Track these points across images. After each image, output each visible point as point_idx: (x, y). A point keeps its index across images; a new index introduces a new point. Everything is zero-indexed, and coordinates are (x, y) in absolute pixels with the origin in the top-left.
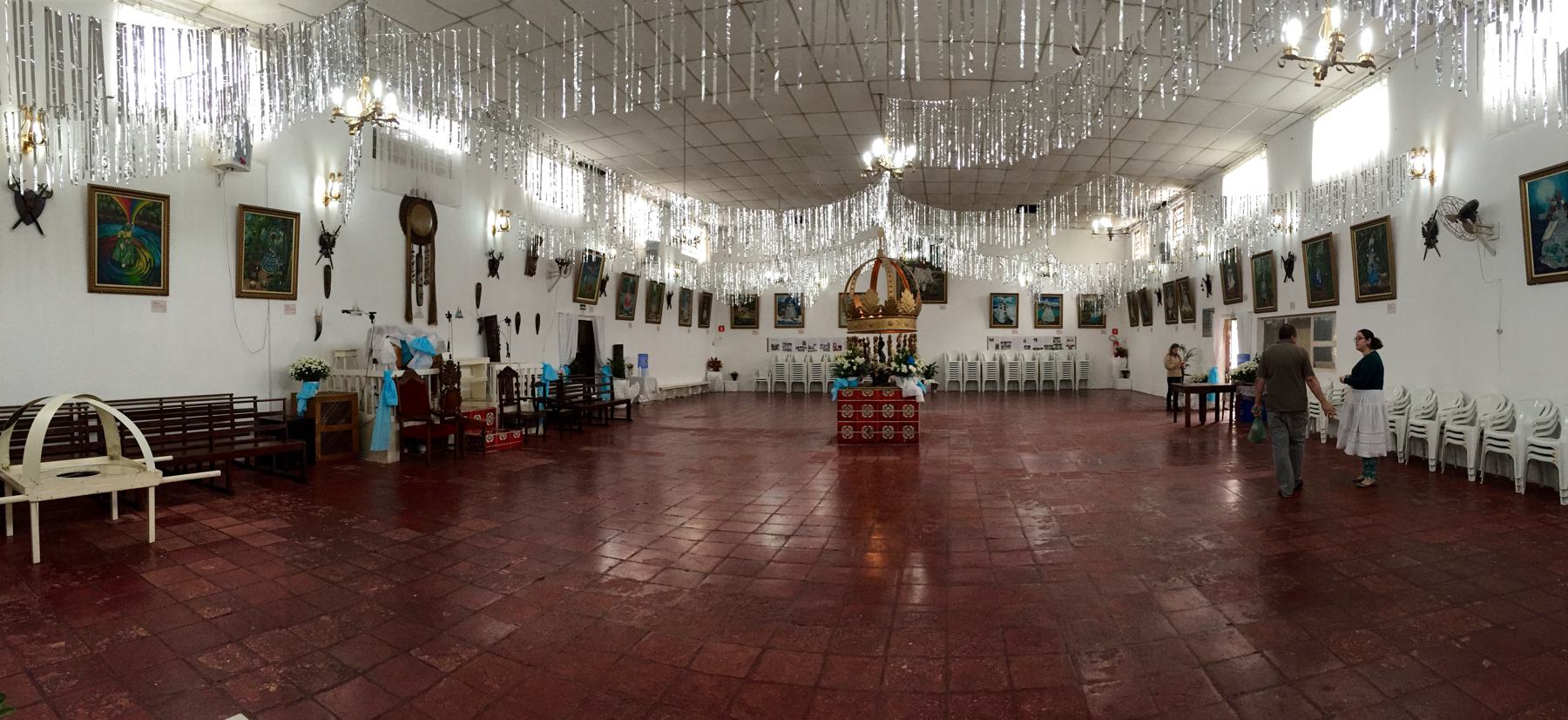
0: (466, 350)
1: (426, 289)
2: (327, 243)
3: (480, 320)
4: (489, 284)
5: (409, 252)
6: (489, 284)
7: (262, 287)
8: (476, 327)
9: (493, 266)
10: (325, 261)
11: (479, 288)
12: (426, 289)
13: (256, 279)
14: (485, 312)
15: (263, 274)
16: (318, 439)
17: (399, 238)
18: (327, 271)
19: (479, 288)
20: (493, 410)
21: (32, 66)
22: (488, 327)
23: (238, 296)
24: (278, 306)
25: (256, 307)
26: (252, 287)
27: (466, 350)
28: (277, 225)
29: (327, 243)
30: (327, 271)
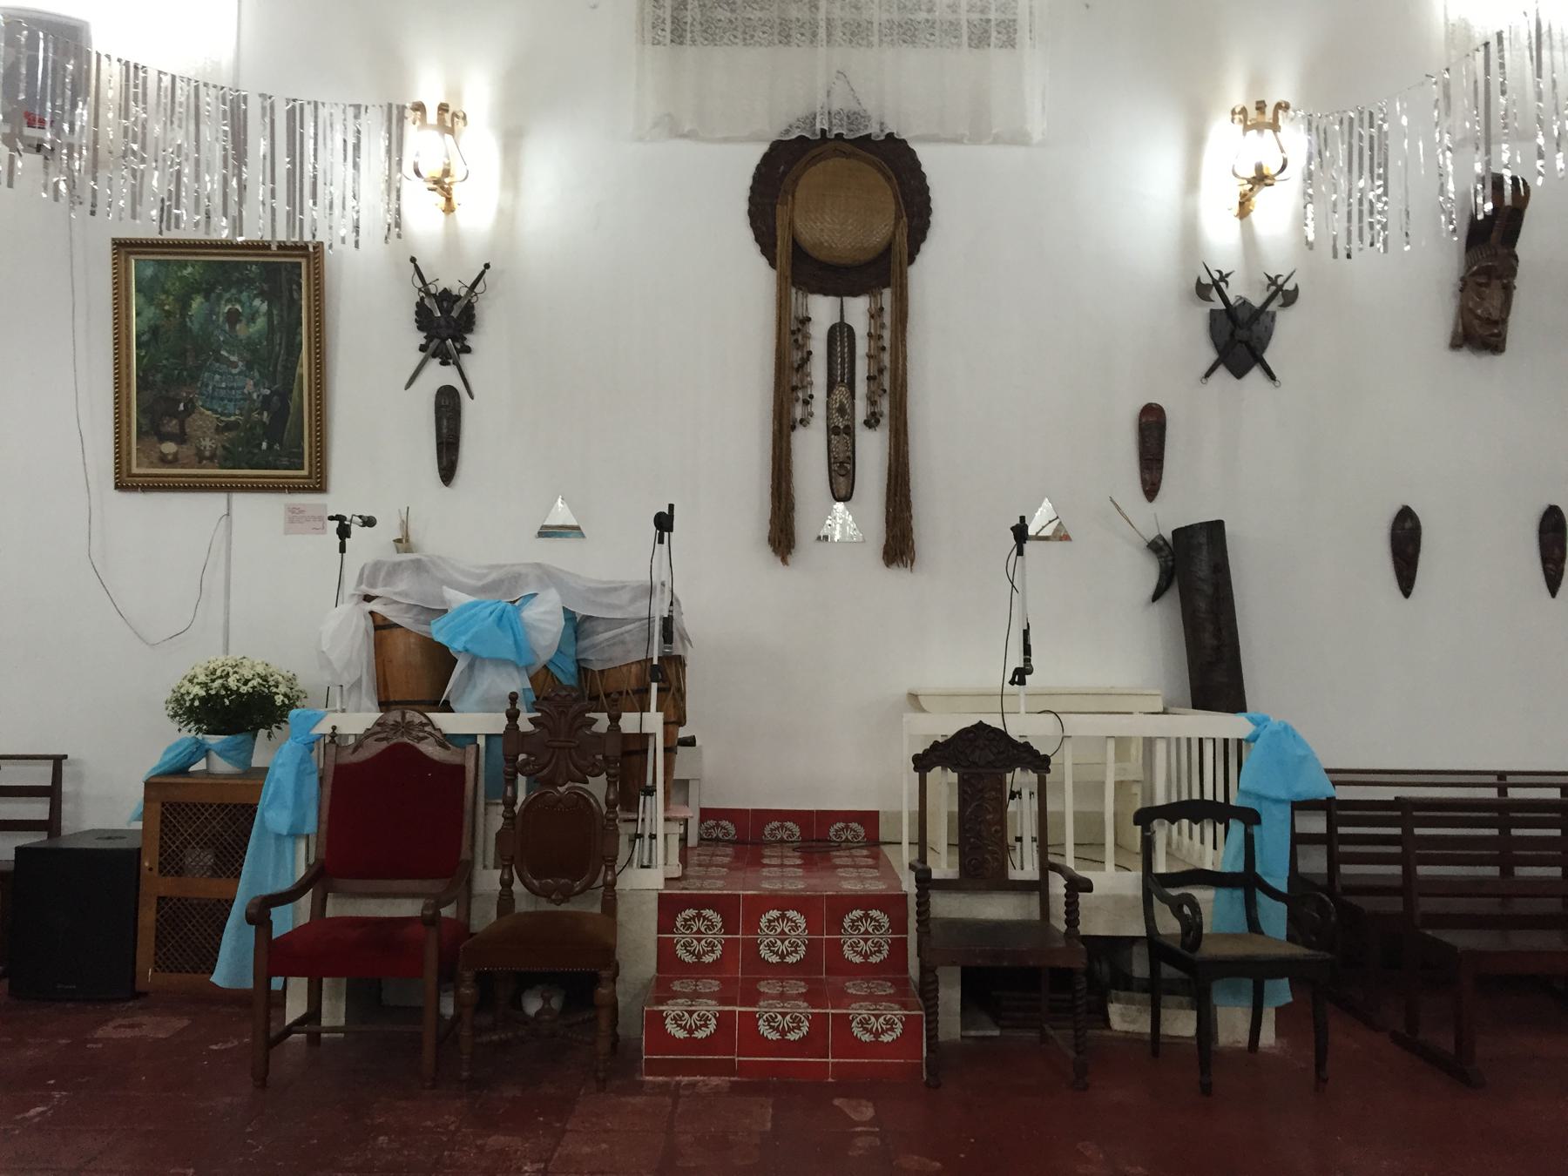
0: (1100, 689)
1: (871, 448)
2: (446, 321)
3: (1155, 546)
4: (1209, 412)
5: (790, 335)
6: (1209, 412)
7: (201, 458)
8: (1147, 572)
9: (1239, 335)
10: (439, 374)
11: (1152, 427)
12: (871, 448)
13: (181, 438)
14: (1178, 508)
15: (203, 423)
16: (148, 918)
17: (752, 279)
18: (448, 407)
19: (1152, 427)
20: (893, 904)
21: (225, 167)
22: (1194, 571)
23: (121, 486)
24: (259, 515)
25: (187, 518)
26: (164, 460)
27: (1100, 689)
28: (244, 283)
29: (446, 321)
30: (448, 407)
